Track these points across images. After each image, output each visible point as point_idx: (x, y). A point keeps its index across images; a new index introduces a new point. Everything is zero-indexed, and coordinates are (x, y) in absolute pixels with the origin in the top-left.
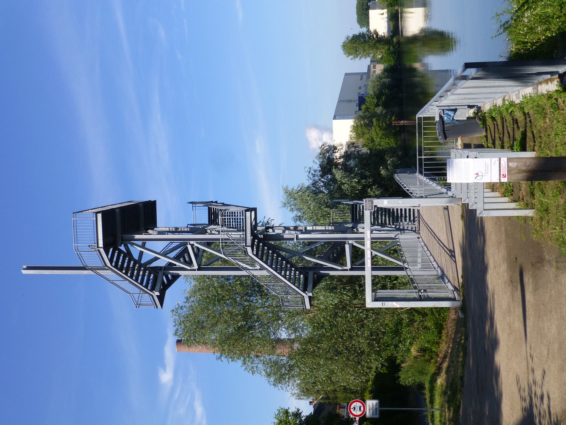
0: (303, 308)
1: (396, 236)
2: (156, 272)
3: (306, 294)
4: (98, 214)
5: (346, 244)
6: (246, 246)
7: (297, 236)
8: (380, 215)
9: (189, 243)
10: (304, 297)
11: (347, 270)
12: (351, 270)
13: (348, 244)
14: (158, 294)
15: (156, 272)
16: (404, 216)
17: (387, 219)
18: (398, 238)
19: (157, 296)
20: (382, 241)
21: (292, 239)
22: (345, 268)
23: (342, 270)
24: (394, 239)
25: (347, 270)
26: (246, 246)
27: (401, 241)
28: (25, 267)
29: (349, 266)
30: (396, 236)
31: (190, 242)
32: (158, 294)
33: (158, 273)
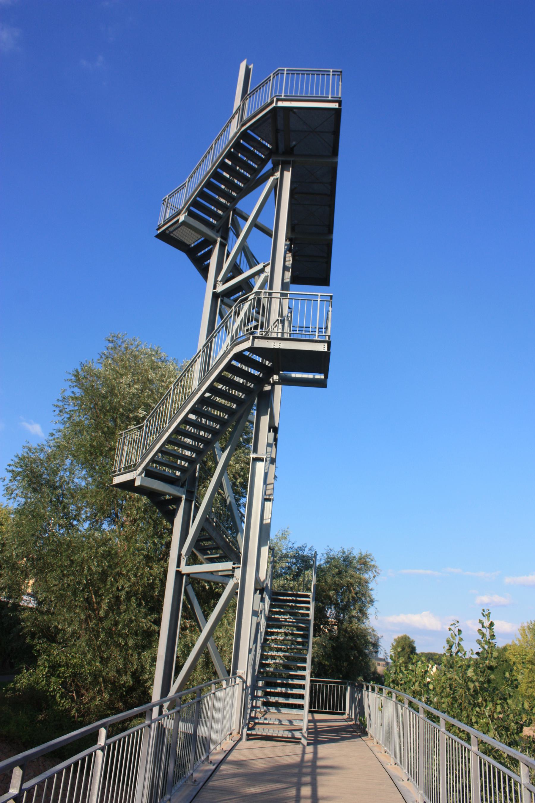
0: (115, 472)
1: (240, 677)
2: (219, 229)
3: (140, 474)
4: (326, 345)
5: (234, 564)
6: (255, 338)
7: (261, 460)
8: (294, 598)
9: (268, 264)
10: (136, 470)
11: (178, 566)
12: (179, 574)
13: (234, 568)
14: (137, 483)
15: (219, 229)
16: (289, 691)
17: (279, 690)
18: (235, 682)
19: (133, 481)
20: (232, 644)
21: (255, 451)
22: (183, 562)
23: (180, 555)
24: (235, 673)
25: (178, 566)
26: (255, 338)
27: (230, 689)
28: (251, 67)
29: (185, 569)
30: (240, 677)
31: (269, 267)
32: (137, 483)
33: (182, 486)
